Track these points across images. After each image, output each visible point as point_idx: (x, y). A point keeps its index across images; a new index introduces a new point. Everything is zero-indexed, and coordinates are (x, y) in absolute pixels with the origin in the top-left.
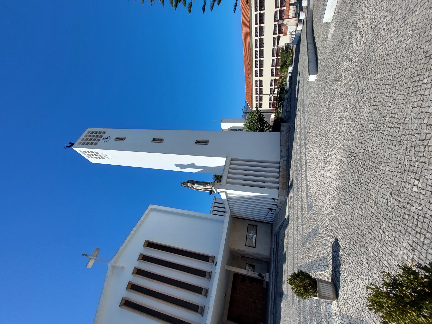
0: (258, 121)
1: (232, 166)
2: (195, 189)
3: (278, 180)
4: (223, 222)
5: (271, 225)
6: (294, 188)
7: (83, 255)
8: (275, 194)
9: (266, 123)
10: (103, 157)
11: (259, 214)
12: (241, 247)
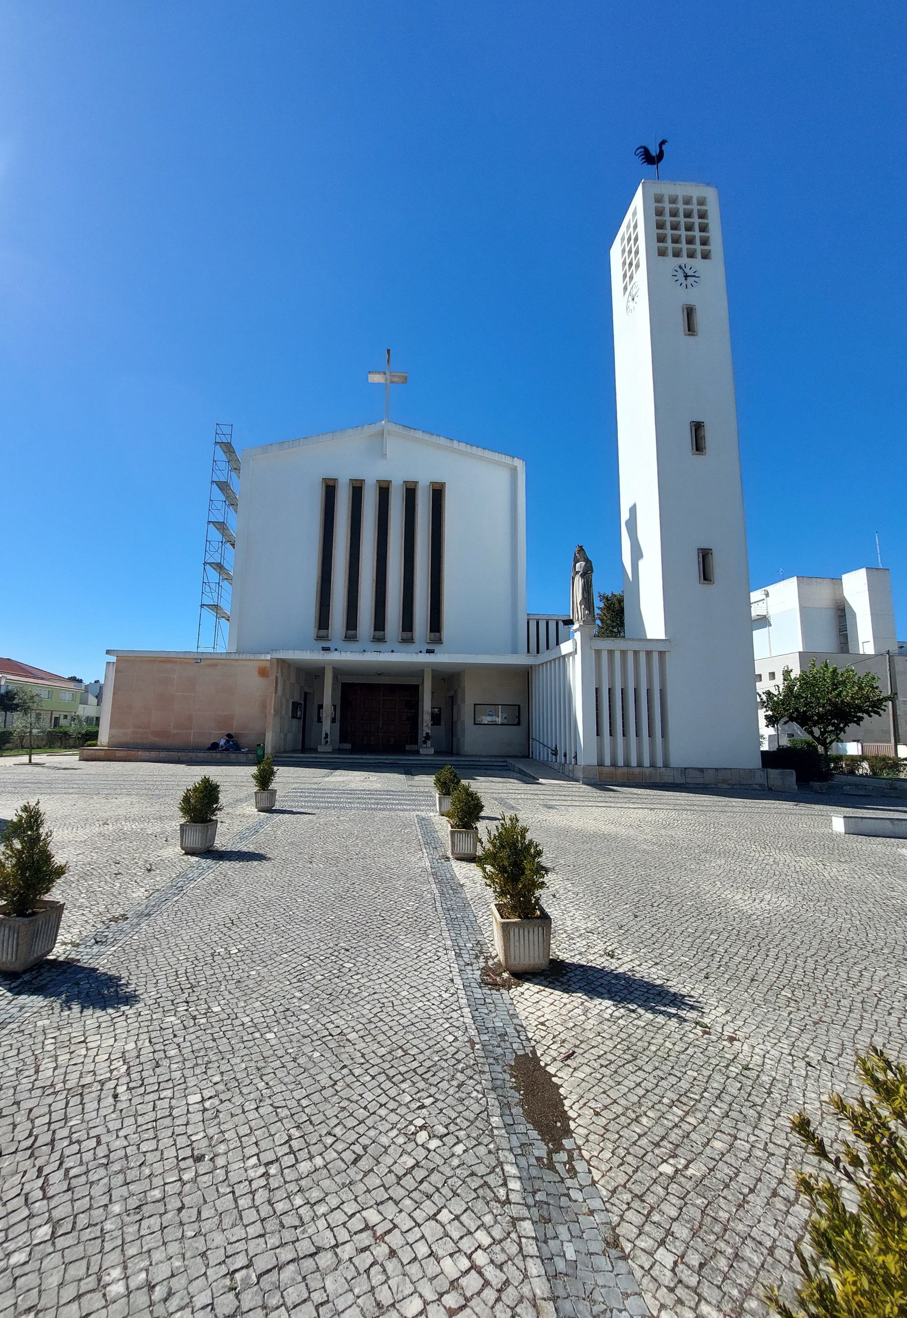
0: (836, 704)
1: (643, 657)
2: (573, 579)
3: (621, 762)
4: (515, 651)
5: (526, 756)
6: (599, 793)
7: (389, 351)
8: (587, 755)
9: (839, 730)
10: (629, 288)
11: (544, 729)
12: (471, 695)
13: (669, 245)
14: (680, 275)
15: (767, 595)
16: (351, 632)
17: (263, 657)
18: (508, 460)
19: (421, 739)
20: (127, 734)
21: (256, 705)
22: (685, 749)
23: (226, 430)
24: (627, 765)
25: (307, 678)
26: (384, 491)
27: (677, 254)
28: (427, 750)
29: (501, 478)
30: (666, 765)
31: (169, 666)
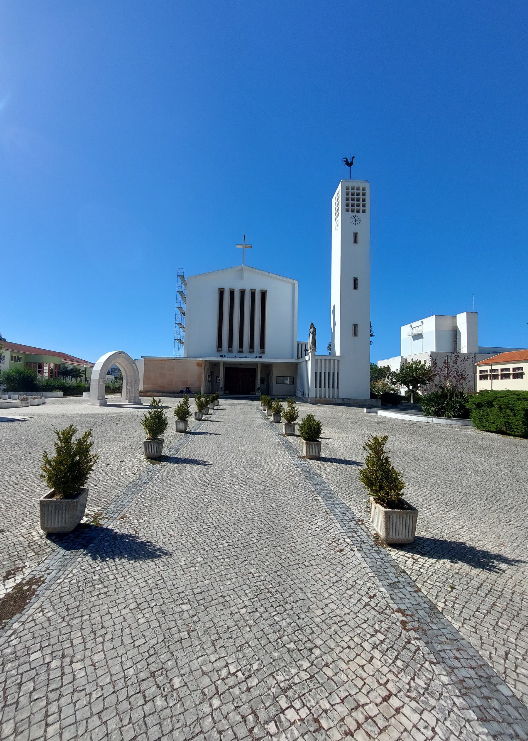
3: (323, 397)
4: (292, 358)
12: (276, 373)
13: (350, 208)
14: (354, 219)
15: (423, 323)
16: (230, 349)
17: (198, 359)
18: (291, 281)
19: (256, 389)
20: (149, 387)
21: (196, 376)
22: (344, 392)
23: (182, 270)
24: (325, 398)
25: (213, 366)
26: (243, 293)
27: (353, 211)
28: (259, 393)
29: (290, 287)
30: (338, 398)
31: (163, 362)
